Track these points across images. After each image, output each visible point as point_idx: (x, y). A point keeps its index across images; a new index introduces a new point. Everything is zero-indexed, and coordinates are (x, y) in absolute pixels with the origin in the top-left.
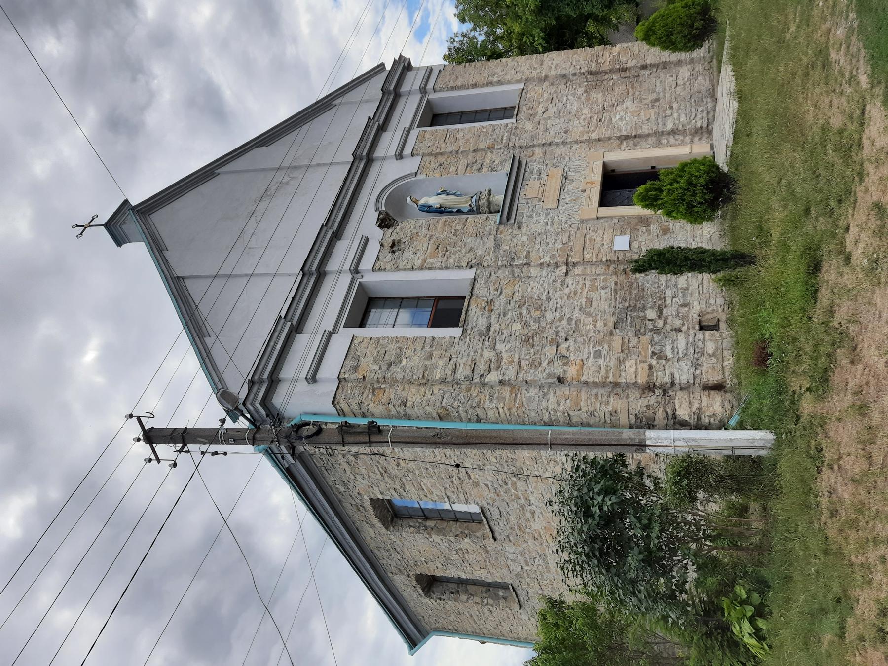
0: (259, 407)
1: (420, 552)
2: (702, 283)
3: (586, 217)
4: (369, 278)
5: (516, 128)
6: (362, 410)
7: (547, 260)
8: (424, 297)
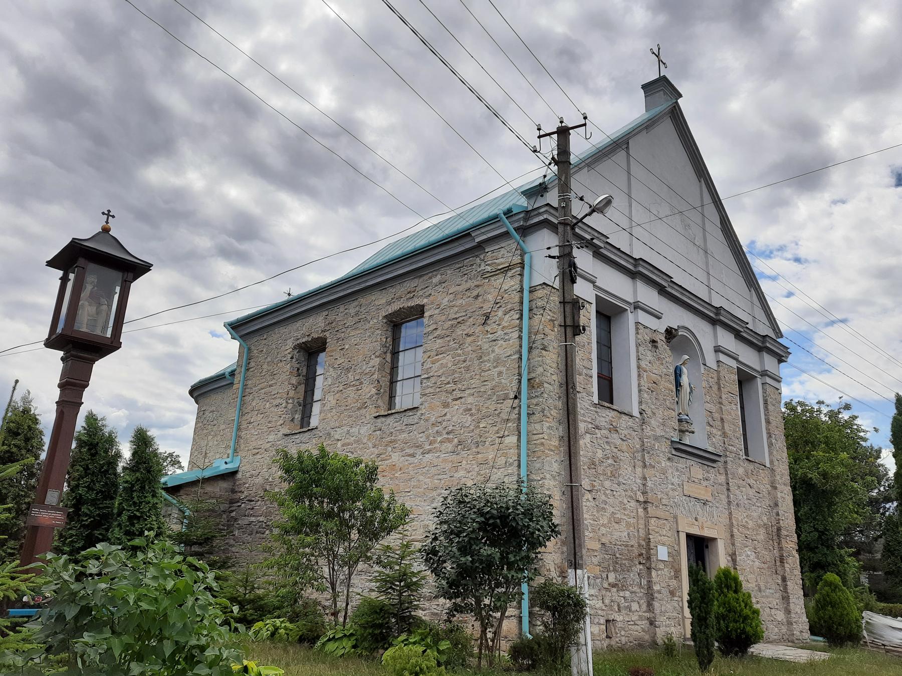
0: (541, 218)
1: (356, 345)
2: (635, 624)
3: (679, 521)
4: (630, 318)
5: (739, 459)
6: (535, 310)
7: (649, 484)
8: (612, 368)
